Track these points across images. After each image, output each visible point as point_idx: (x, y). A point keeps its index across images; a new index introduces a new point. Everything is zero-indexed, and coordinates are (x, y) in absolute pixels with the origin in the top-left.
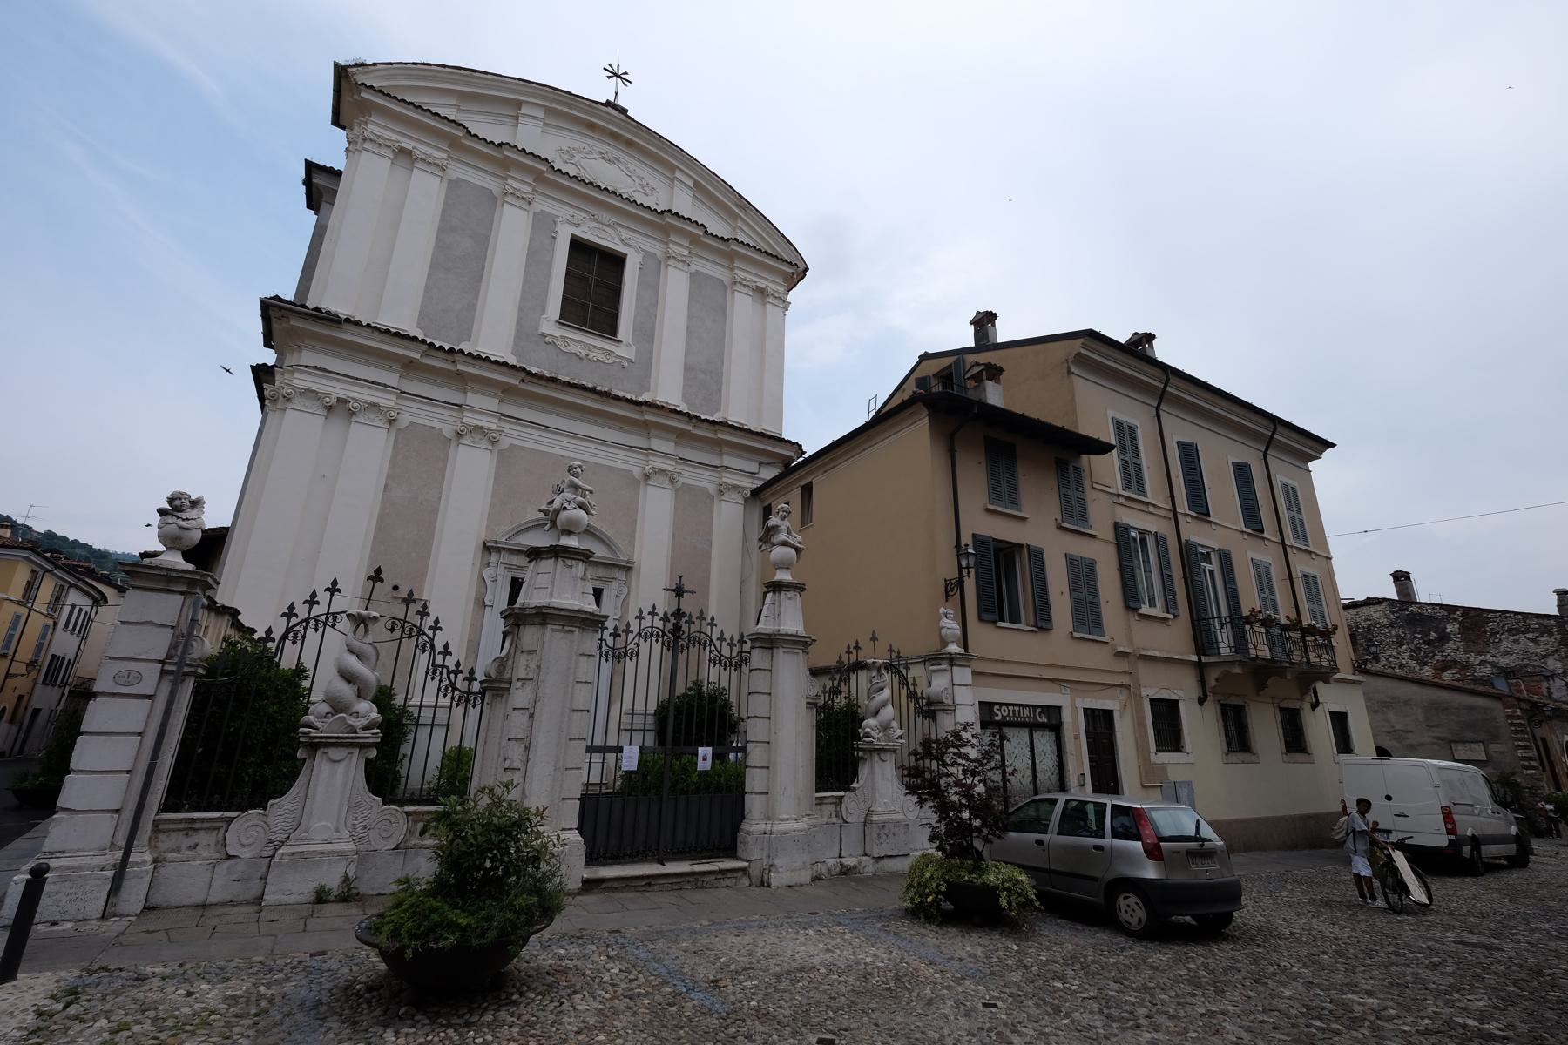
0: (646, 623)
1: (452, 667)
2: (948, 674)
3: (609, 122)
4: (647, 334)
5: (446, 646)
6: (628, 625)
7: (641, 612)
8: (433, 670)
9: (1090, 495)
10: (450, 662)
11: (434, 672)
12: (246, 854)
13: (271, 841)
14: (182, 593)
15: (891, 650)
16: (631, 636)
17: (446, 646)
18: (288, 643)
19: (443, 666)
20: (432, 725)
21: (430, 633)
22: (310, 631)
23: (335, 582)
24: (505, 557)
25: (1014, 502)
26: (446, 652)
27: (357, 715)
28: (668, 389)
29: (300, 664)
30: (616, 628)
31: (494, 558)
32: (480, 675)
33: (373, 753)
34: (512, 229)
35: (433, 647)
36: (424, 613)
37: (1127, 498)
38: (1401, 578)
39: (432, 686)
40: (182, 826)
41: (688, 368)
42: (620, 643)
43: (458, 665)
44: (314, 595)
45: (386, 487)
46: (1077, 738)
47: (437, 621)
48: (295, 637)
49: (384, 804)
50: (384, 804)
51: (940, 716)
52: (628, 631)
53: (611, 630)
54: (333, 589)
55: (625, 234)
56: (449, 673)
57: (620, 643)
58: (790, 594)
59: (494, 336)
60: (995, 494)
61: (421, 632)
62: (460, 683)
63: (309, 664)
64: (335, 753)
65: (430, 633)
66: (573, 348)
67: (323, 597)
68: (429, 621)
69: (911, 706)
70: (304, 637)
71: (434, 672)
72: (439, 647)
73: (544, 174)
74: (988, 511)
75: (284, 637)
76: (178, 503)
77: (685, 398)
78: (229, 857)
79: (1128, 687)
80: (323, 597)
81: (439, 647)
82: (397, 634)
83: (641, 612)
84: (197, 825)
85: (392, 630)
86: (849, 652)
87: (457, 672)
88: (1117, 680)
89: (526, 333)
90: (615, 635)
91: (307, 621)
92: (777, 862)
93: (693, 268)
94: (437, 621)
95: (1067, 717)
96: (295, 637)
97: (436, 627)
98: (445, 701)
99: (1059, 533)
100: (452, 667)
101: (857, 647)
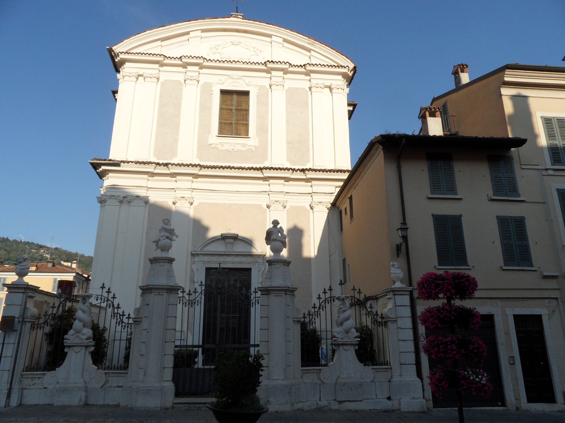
0: (328, 295)
1: (121, 314)
2: (392, 301)
3: (233, 24)
4: (263, 130)
5: (118, 305)
6: (196, 289)
7: (325, 290)
8: (114, 315)
9: (519, 173)
10: (120, 311)
11: (114, 316)
14: (23, 293)
15: (354, 289)
16: (197, 294)
17: (118, 305)
19: (117, 313)
20: (120, 340)
21: (112, 300)
22: (327, 304)
23: (103, 284)
24: (201, 258)
25: (452, 189)
26: (118, 307)
27: (83, 334)
28: (278, 157)
29: (104, 327)
30: (190, 291)
31: (197, 259)
32: (132, 316)
33: (92, 349)
34: (191, 97)
35: (113, 305)
36: (109, 292)
37: (554, 170)
38: (154, 242)
39: (114, 321)
40: (30, 376)
41: (289, 143)
42: (192, 297)
43: (123, 312)
44: (319, 295)
46: (507, 334)
47: (114, 295)
49: (364, 365)
50: (364, 365)
51: (389, 324)
52: (195, 292)
53: (187, 292)
54: (330, 289)
55: (247, 80)
56: (120, 315)
57: (192, 297)
58: (277, 266)
59: (187, 152)
60: (435, 186)
61: (108, 300)
62: (125, 320)
63: (107, 326)
64: (76, 349)
65: (112, 300)
66: (226, 147)
68: (111, 295)
71: (114, 316)
72: (116, 306)
73: (201, 64)
74: (429, 198)
76: (19, 260)
77: (289, 160)
79: (557, 299)
81: (116, 306)
83: (325, 290)
84: (34, 376)
85: (97, 300)
86: (325, 292)
87: (123, 315)
88: (546, 294)
89: (203, 146)
90: (189, 294)
91: (325, 300)
92: (271, 400)
93: (286, 87)
94: (114, 295)
95: (498, 320)
97: (114, 297)
98: (119, 328)
99: (491, 203)
100: (121, 314)
101: (330, 289)
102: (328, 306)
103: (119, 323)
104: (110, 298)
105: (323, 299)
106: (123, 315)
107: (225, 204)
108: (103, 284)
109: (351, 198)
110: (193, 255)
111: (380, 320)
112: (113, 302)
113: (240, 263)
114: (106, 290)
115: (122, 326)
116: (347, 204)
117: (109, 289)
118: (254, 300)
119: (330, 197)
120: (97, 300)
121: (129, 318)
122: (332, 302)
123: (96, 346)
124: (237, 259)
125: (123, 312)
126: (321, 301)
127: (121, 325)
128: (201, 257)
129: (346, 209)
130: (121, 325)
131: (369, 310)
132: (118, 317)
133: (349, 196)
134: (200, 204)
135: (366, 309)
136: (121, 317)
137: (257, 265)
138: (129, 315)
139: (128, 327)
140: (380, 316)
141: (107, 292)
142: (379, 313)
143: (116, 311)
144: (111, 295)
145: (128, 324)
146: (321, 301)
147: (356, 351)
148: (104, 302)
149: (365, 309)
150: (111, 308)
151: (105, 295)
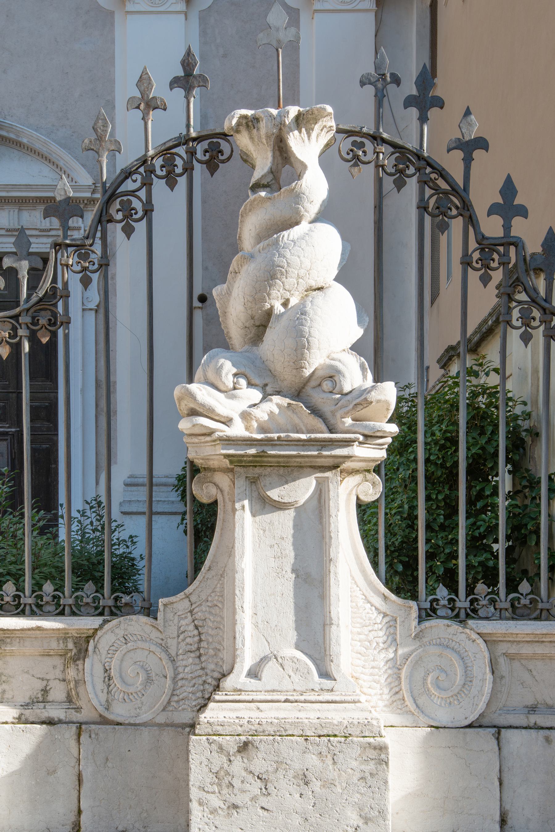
70: (148, 211)
81: (484, 195)
122: (199, 170)
135: (471, 220)
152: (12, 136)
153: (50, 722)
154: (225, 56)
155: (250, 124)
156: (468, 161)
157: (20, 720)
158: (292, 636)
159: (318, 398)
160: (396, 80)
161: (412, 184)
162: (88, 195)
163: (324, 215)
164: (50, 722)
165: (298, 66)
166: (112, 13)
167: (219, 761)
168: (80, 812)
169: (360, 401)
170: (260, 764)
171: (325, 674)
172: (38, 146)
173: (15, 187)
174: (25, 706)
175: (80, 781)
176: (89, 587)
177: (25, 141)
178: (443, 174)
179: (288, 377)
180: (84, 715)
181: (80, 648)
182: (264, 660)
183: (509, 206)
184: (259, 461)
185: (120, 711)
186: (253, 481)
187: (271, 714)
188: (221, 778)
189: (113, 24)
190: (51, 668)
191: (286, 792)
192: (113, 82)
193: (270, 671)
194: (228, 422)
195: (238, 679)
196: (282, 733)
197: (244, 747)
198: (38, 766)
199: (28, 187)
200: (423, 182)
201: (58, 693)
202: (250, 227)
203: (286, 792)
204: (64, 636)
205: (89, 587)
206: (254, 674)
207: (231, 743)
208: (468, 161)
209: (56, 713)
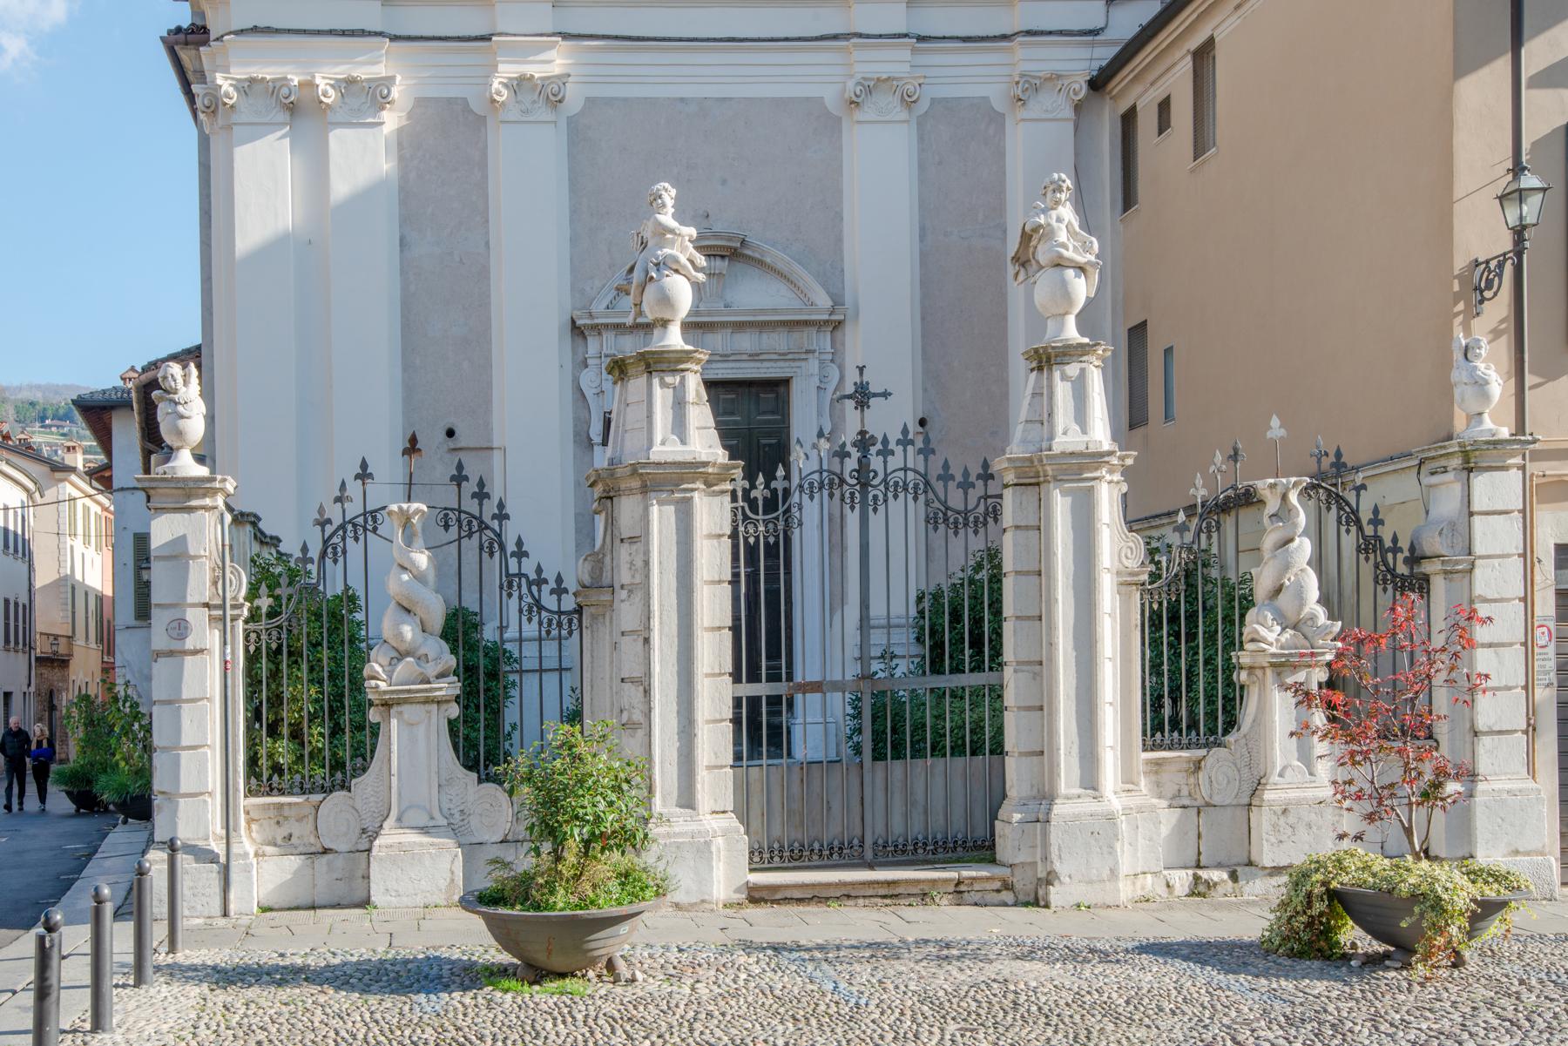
5: (519, 543)
8: (509, 582)
10: (529, 567)
11: (510, 585)
12: (342, 846)
13: (364, 831)
17: (519, 543)
18: (329, 562)
21: (495, 525)
22: (350, 541)
23: (364, 465)
26: (521, 554)
30: (966, 473)
35: (502, 547)
36: (481, 495)
43: (539, 570)
44: (321, 510)
45: (403, 243)
47: (501, 505)
48: (335, 553)
49: (480, 781)
50: (480, 781)
54: (364, 475)
56: (530, 584)
61: (483, 526)
62: (549, 601)
67: (354, 489)
68: (490, 508)
69: (1367, 569)
70: (344, 552)
75: (323, 554)
78: (326, 851)
80: (354, 489)
81: (1366, 515)
82: (454, 530)
85: (447, 527)
87: (541, 582)
91: (342, 527)
96: (335, 553)
97: (502, 516)
100: (533, 576)
102: (354, 549)
103: (530, 611)
104: (487, 518)
105: (337, 521)
106: (541, 582)
107: (682, 100)
108: (364, 465)
109: (1204, 55)
110: (577, 331)
111: (1402, 569)
112: (499, 536)
113: (754, 357)
114: (470, 487)
115: (540, 623)
116: (1177, 80)
117: (481, 484)
118: (981, 509)
119: (1084, 53)
120: (447, 527)
121: (559, 591)
123: (468, 698)
124: (746, 342)
125: (539, 570)
126: (329, 529)
127: (535, 619)
128: (608, 337)
129: (1164, 106)
130: (535, 619)
131: (1369, 530)
132: (524, 590)
133: (1195, 42)
134: (590, 101)
135: (1360, 528)
136: (534, 589)
137: (813, 365)
138: (559, 580)
139: (560, 625)
140: (553, 585)
141: (474, 495)
142: (1404, 544)
143: (513, 569)
144: (490, 508)
145: (560, 613)
146: (329, 529)
147: (452, 724)
148: (470, 536)
149: (1354, 529)
150: (497, 555)
151: (471, 506)
152: (757, 255)
153: (1184, 807)
154: (940, 163)
155: (1273, 486)
156: (1358, 496)
157: (1170, 806)
158: (1296, 755)
159: (1306, 629)
160: (1327, 454)
161: (1334, 507)
162: (826, 317)
163: (1305, 533)
164: (1184, 807)
165: (1004, 173)
166: (840, 119)
167: (1274, 818)
168: (1199, 854)
169: (1323, 631)
170: (1292, 819)
171: (1311, 774)
172: (780, 266)
173: (762, 311)
174: (1173, 798)
175: (1199, 836)
176: (1158, 735)
177: (768, 260)
178: (1348, 504)
179: (1293, 619)
180: (1200, 802)
181: (1198, 765)
182: (1284, 768)
183: (1376, 521)
184: (1281, 665)
185: (1216, 800)
186: (1279, 674)
187: (1293, 794)
188: (1275, 826)
189: (840, 131)
190: (1181, 778)
191: (1302, 832)
192: (841, 192)
193: (1288, 772)
194: (1271, 644)
195: (1275, 778)
196: (1299, 802)
197: (1285, 811)
198: (1179, 830)
199: (775, 311)
200: (1340, 508)
201: (1185, 792)
202: (1269, 542)
203: (1302, 832)
204: (1189, 760)
205: (1176, 734)
206: (1281, 775)
207: (1279, 809)
208: (1358, 496)
209: (1186, 802)
